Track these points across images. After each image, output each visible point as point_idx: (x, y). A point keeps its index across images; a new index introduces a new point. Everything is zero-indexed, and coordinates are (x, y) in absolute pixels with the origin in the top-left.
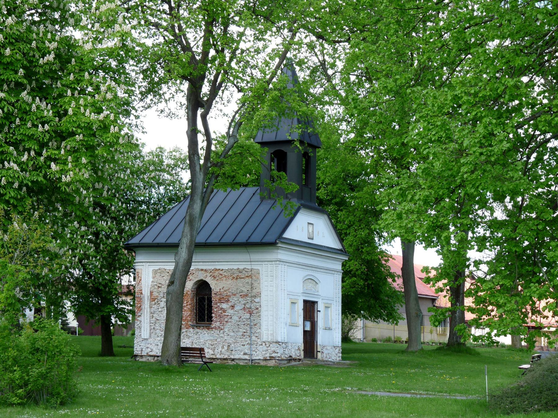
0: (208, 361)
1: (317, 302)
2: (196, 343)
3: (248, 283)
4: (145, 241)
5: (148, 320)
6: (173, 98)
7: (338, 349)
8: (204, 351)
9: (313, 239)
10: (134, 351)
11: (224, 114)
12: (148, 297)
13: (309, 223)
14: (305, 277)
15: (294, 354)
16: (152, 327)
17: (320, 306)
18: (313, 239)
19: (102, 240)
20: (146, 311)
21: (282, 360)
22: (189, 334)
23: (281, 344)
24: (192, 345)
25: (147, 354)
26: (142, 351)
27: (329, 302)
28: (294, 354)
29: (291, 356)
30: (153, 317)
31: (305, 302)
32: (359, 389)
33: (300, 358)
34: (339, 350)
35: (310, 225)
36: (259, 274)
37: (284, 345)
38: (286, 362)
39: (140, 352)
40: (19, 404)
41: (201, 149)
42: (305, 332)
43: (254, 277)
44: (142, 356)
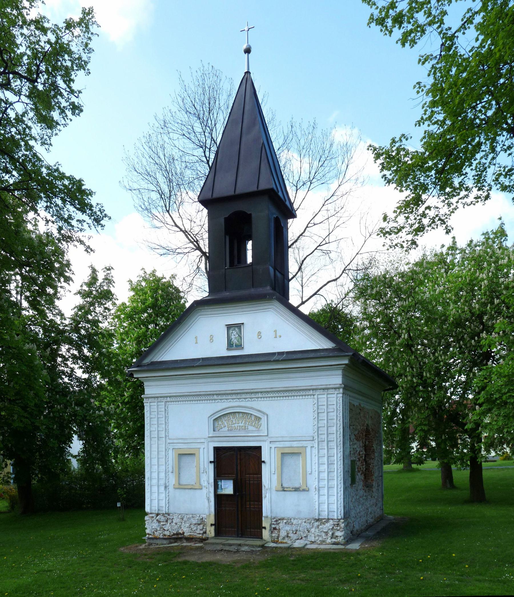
9: (240, 346)
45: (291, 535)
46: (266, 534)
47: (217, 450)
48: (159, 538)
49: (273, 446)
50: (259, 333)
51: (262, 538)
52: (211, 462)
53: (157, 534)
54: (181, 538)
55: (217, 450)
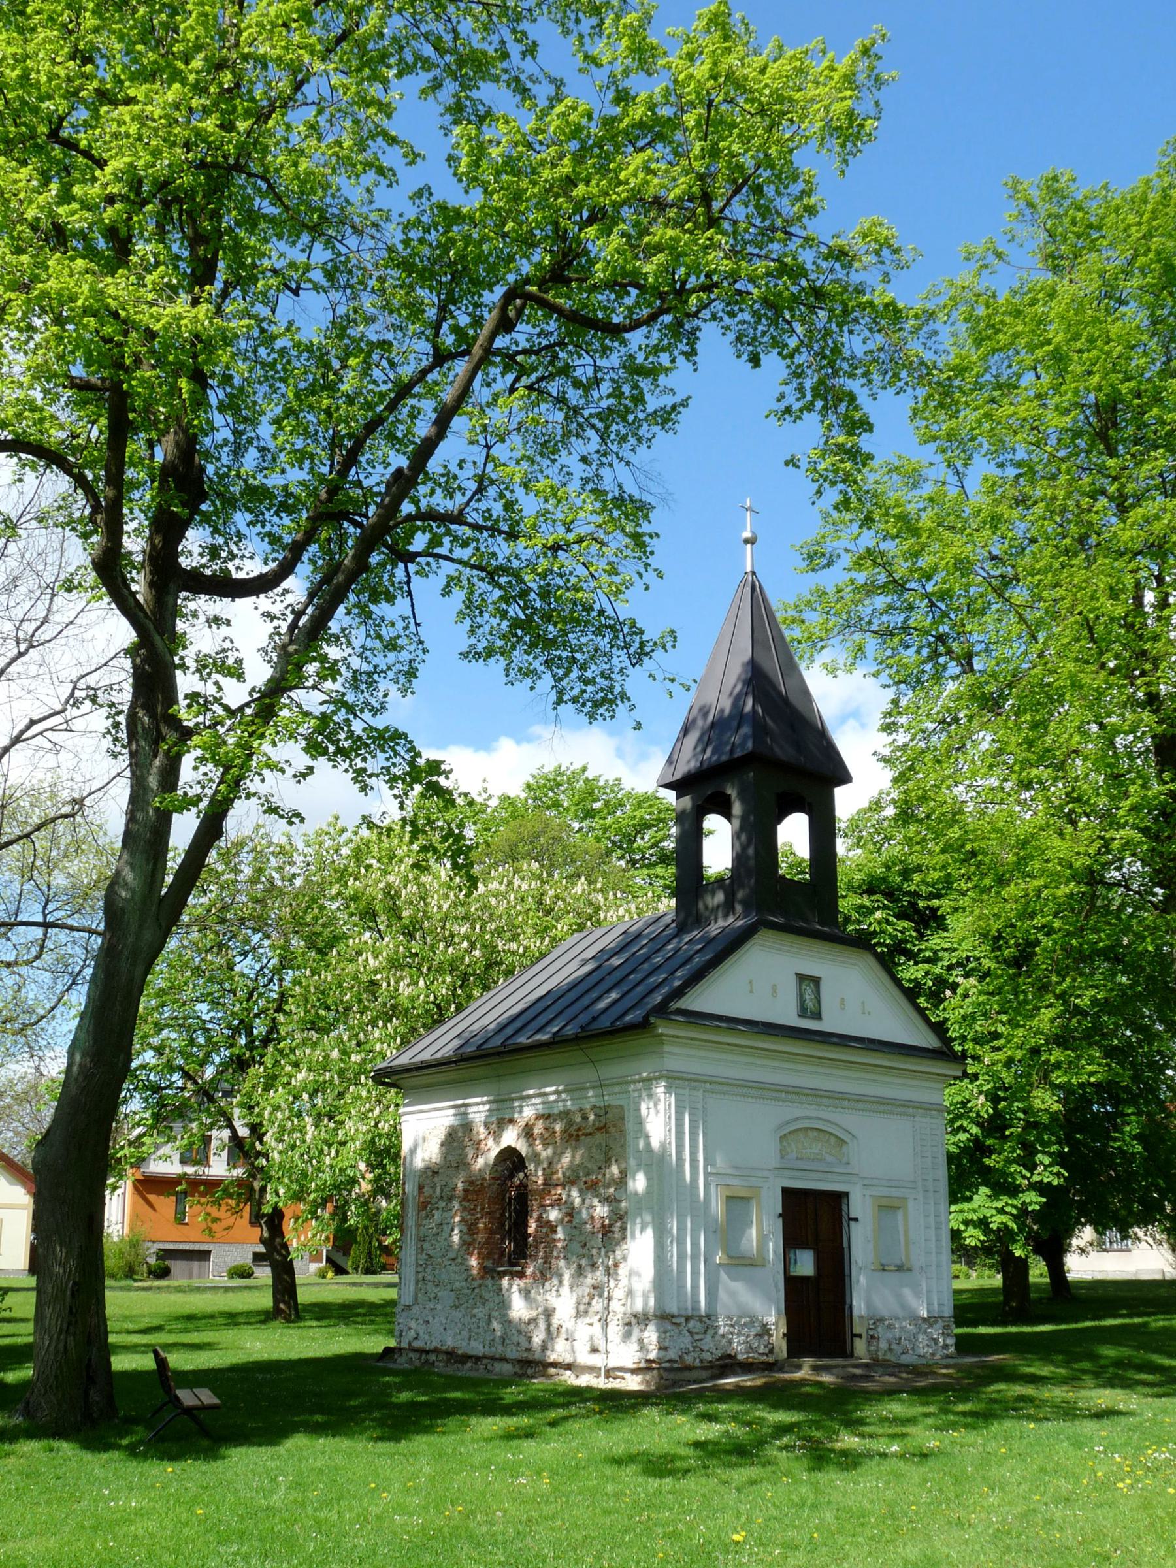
1: (846, 1194)
9: (817, 1016)
14: (781, 1126)
17: (859, 1205)
21: (689, 1368)
27: (895, 1192)
33: (771, 1359)
36: (623, 1119)
38: (704, 1374)
42: (793, 1285)
43: (612, 1130)
45: (894, 1347)
46: (860, 1347)
47: (787, 1193)
48: (695, 1368)
49: (868, 1193)
50: (843, 1001)
51: (852, 1355)
52: (856, 1220)
53: (689, 1359)
54: (732, 1365)
55: (787, 1193)
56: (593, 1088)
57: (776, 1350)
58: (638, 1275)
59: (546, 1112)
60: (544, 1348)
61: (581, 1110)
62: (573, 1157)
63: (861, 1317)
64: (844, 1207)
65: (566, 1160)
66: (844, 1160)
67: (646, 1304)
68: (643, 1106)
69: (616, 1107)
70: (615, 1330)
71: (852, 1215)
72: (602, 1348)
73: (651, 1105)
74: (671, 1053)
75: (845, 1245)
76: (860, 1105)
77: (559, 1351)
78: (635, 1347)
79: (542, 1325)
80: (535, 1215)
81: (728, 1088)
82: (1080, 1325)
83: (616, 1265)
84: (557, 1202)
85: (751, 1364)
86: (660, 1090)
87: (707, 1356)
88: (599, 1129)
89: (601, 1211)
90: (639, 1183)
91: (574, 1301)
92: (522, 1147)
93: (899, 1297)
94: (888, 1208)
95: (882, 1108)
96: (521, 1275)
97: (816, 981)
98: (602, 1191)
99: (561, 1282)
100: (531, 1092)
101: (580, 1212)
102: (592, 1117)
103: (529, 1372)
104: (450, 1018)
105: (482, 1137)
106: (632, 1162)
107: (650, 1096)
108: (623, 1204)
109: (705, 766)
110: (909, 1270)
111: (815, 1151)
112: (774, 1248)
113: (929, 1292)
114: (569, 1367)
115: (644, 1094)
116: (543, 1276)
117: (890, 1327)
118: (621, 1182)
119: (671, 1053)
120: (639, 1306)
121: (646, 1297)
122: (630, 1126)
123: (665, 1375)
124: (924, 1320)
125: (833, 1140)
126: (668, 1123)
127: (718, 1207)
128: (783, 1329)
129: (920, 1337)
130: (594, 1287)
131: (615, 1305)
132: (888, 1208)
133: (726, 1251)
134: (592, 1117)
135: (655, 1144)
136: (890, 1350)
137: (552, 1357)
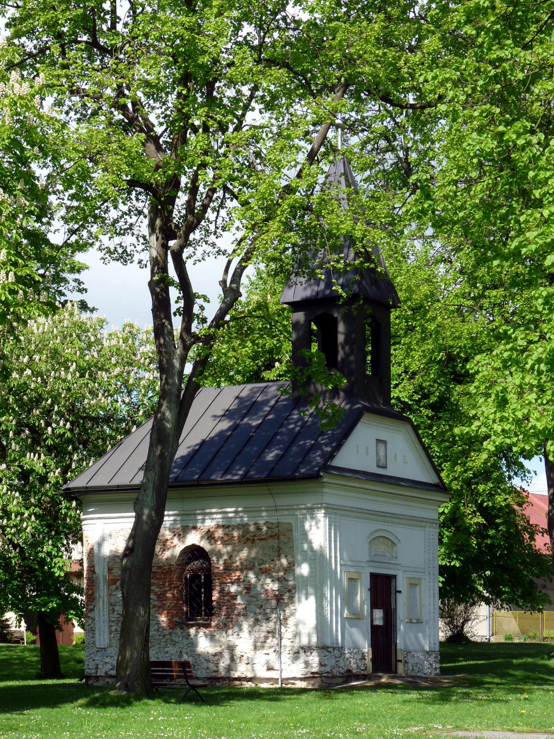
0: (200, 683)
1: (395, 577)
2: (187, 653)
3: (273, 547)
4: (96, 483)
5: (106, 617)
6: (131, 229)
7: (434, 655)
8: (190, 667)
9: (385, 467)
10: (84, 670)
11: (218, 252)
12: (104, 577)
13: (378, 441)
14: (372, 533)
15: (354, 666)
16: (113, 628)
17: (401, 584)
18: (385, 467)
19: (33, 486)
20: (101, 600)
21: (334, 677)
22: (174, 638)
23: (329, 650)
24: (181, 655)
25: (106, 673)
26: (97, 668)
27: (417, 575)
28: (354, 666)
29: (349, 671)
30: (113, 611)
31: (374, 577)
32: (457, 728)
33: (366, 673)
34: (436, 657)
35: (380, 444)
36: (291, 531)
37: (336, 651)
38: (340, 680)
39: (93, 671)
40: (486, 700)
41: (175, 314)
42: (374, 629)
43: (282, 538)
44: (98, 677)
45: (415, 668)
52: (400, 592)
56: (266, 511)
57: (368, 668)
58: (304, 624)
59: (226, 524)
60: (229, 669)
61: (256, 524)
62: (249, 552)
63: (401, 650)
64: (393, 583)
65: (244, 554)
66: (394, 556)
67: (310, 641)
68: (307, 525)
69: (285, 523)
70: (286, 656)
71: (398, 589)
72: (277, 666)
73: (313, 523)
74: (327, 493)
75: (393, 607)
76: (403, 521)
77: (241, 670)
78: (303, 665)
79: (227, 655)
80: (218, 588)
81: (351, 514)
82: (475, 662)
83: (286, 619)
84: (238, 581)
85: (358, 675)
86: (320, 514)
87: (342, 671)
88: (271, 536)
89: (272, 586)
90: (304, 569)
91: (252, 641)
92: (205, 545)
93: (417, 638)
94: (413, 585)
95: (412, 522)
96: (207, 626)
97: (385, 442)
98: (274, 574)
99: (241, 630)
100: (214, 510)
101: (255, 587)
102: (265, 529)
103: (218, 684)
104: (109, 452)
105: (169, 537)
106: (299, 557)
107: (312, 518)
108: (291, 583)
109: (320, 296)
110: (421, 622)
111: (382, 550)
112: (366, 608)
113: (430, 636)
114: (250, 680)
115: (308, 517)
116: (225, 627)
117: (413, 656)
118: (290, 569)
119: (327, 493)
120: (305, 641)
121: (309, 636)
122: (296, 534)
123: (325, 680)
124: (427, 652)
125: (390, 543)
126: (325, 536)
127: (345, 583)
128: (371, 656)
129: (426, 663)
130: (269, 632)
131: (285, 642)
132: (413, 585)
133: (349, 610)
134: (265, 529)
135: (316, 546)
136: (413, 670)
137: (236, 675)
